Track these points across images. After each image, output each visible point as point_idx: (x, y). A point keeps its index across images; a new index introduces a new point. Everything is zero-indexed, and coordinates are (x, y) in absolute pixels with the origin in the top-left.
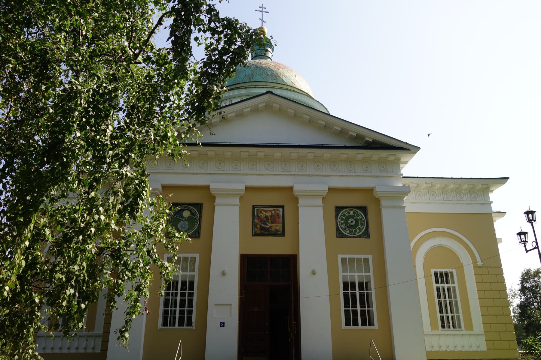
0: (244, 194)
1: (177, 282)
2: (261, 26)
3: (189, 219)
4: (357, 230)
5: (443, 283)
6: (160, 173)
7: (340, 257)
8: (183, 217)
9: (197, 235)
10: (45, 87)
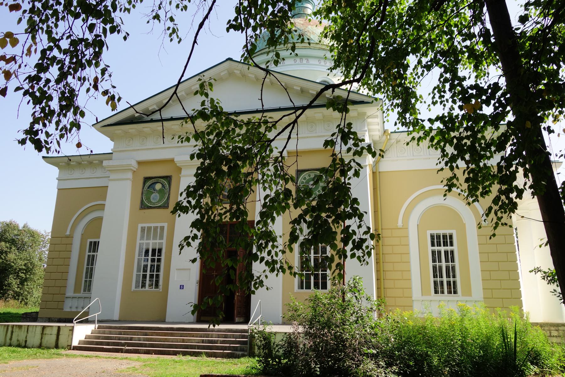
3: (160, 191)
5: (439, 245)
7: (140, 226)
9: (166, 205)
10: (383, 46)
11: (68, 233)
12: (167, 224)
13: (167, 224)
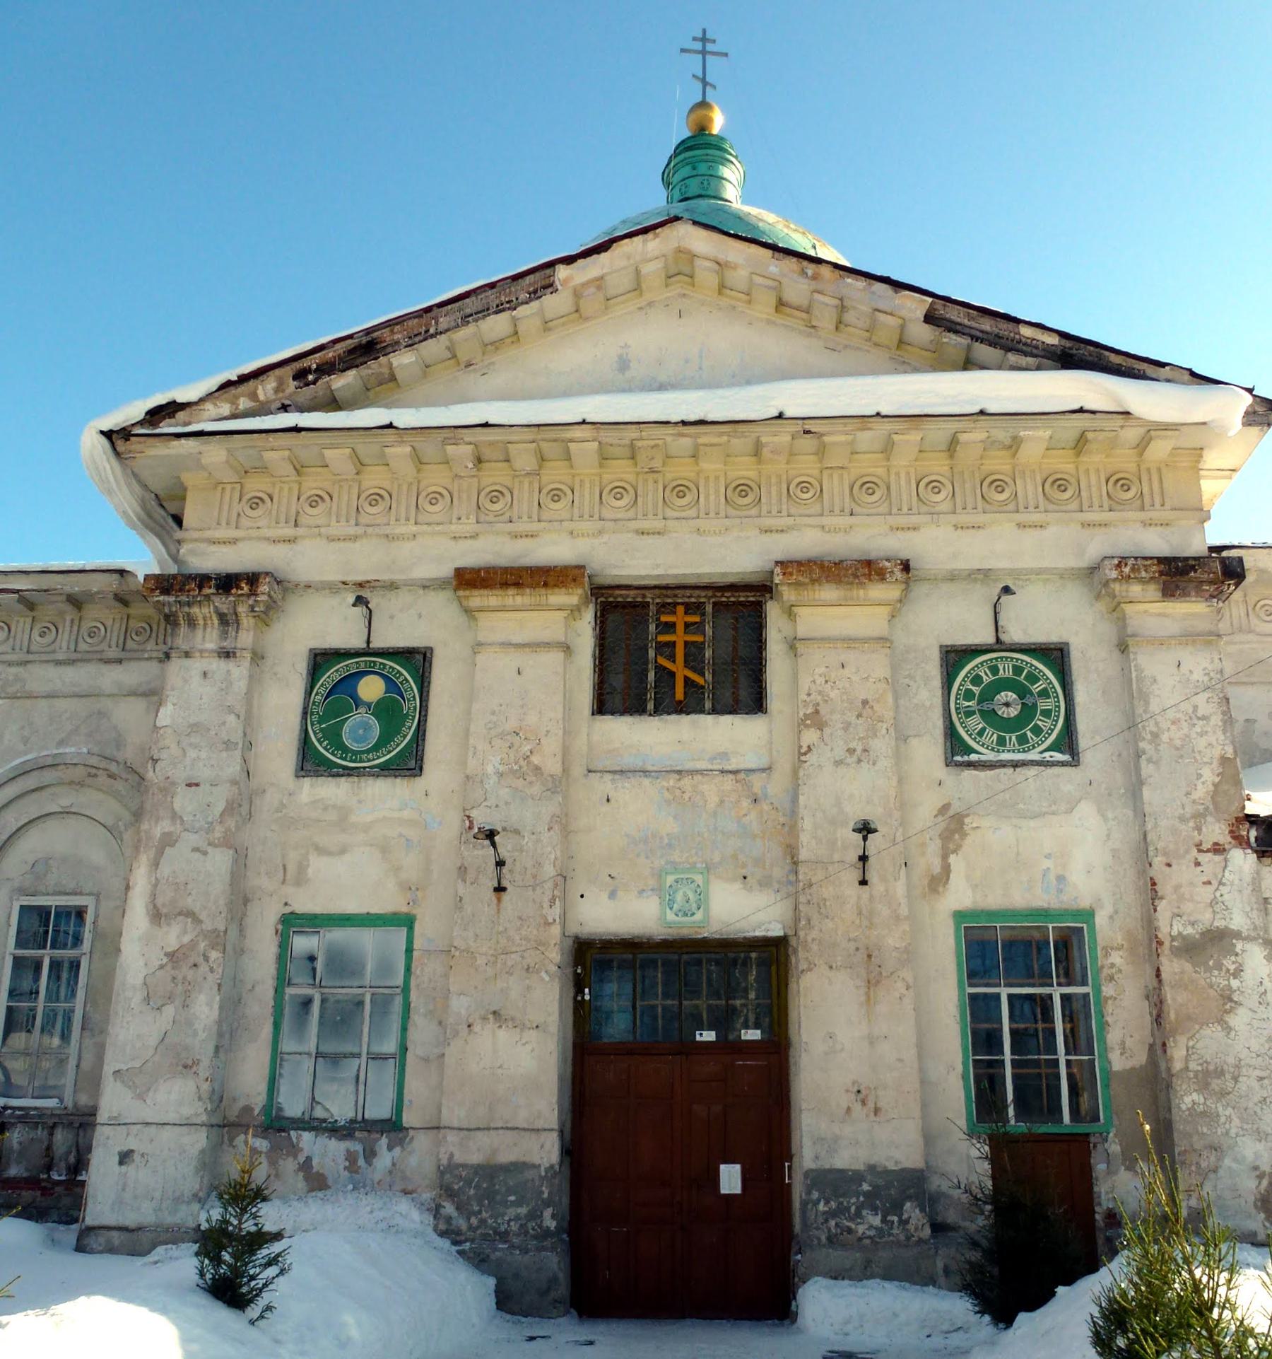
2: (700, 99)
4: (1029, 733)
8: (358, 702)
9: (412, 764)
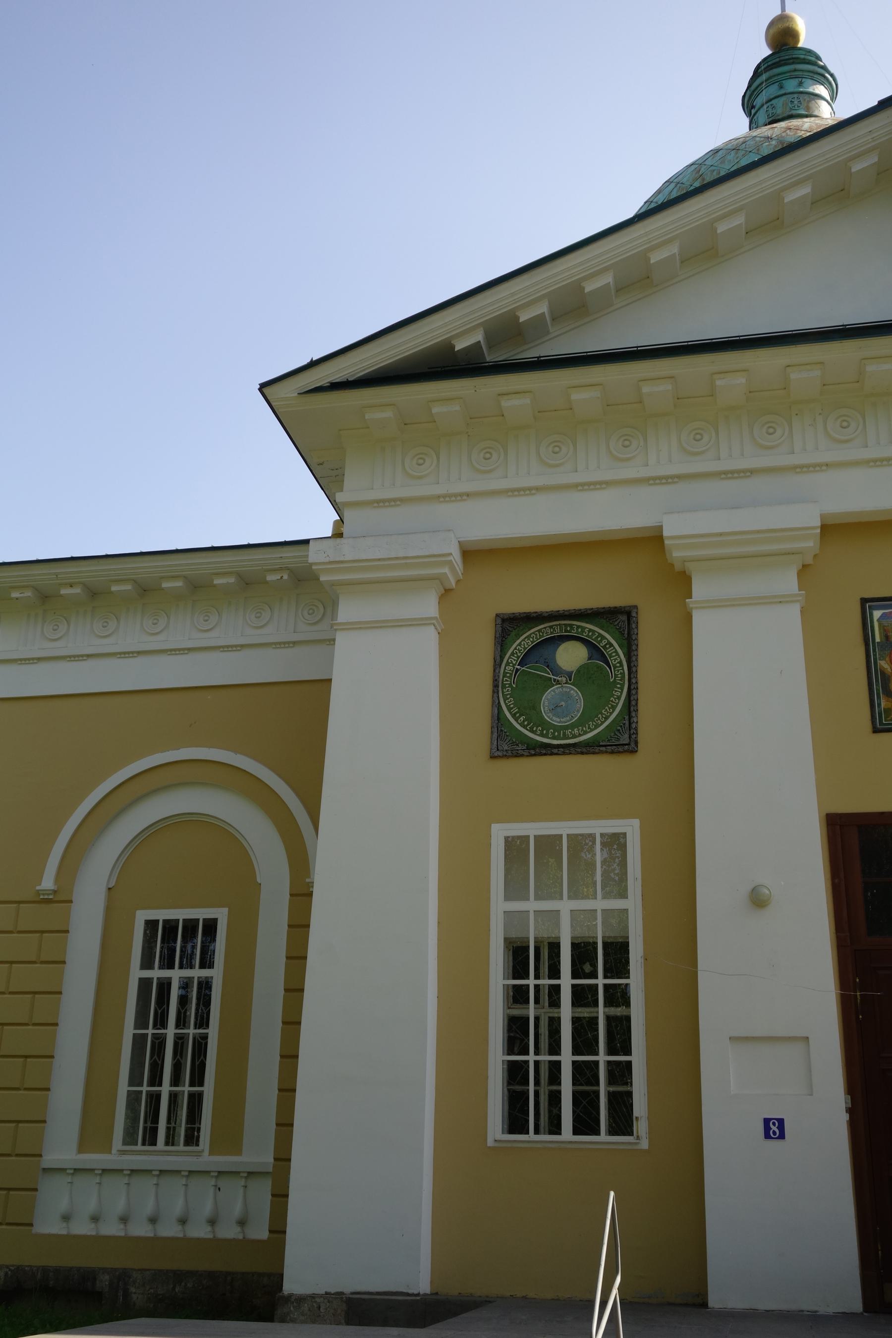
0: (815, 556)
1: (555, 947)
3: (581, 677)
6: (450, 496)
8: (556, 670)
9: (625, 739)
11: (48, 883)
12: (636, 822)
13: (636, 822)
